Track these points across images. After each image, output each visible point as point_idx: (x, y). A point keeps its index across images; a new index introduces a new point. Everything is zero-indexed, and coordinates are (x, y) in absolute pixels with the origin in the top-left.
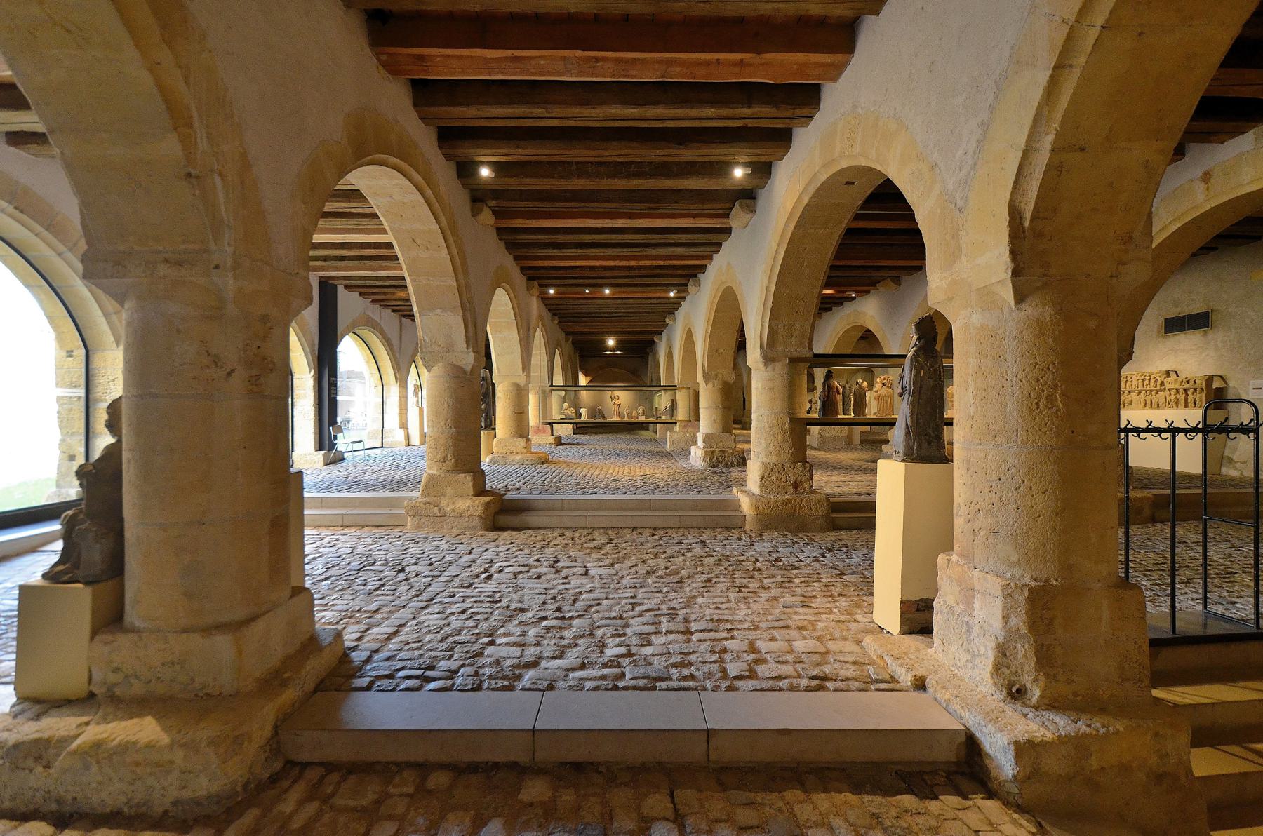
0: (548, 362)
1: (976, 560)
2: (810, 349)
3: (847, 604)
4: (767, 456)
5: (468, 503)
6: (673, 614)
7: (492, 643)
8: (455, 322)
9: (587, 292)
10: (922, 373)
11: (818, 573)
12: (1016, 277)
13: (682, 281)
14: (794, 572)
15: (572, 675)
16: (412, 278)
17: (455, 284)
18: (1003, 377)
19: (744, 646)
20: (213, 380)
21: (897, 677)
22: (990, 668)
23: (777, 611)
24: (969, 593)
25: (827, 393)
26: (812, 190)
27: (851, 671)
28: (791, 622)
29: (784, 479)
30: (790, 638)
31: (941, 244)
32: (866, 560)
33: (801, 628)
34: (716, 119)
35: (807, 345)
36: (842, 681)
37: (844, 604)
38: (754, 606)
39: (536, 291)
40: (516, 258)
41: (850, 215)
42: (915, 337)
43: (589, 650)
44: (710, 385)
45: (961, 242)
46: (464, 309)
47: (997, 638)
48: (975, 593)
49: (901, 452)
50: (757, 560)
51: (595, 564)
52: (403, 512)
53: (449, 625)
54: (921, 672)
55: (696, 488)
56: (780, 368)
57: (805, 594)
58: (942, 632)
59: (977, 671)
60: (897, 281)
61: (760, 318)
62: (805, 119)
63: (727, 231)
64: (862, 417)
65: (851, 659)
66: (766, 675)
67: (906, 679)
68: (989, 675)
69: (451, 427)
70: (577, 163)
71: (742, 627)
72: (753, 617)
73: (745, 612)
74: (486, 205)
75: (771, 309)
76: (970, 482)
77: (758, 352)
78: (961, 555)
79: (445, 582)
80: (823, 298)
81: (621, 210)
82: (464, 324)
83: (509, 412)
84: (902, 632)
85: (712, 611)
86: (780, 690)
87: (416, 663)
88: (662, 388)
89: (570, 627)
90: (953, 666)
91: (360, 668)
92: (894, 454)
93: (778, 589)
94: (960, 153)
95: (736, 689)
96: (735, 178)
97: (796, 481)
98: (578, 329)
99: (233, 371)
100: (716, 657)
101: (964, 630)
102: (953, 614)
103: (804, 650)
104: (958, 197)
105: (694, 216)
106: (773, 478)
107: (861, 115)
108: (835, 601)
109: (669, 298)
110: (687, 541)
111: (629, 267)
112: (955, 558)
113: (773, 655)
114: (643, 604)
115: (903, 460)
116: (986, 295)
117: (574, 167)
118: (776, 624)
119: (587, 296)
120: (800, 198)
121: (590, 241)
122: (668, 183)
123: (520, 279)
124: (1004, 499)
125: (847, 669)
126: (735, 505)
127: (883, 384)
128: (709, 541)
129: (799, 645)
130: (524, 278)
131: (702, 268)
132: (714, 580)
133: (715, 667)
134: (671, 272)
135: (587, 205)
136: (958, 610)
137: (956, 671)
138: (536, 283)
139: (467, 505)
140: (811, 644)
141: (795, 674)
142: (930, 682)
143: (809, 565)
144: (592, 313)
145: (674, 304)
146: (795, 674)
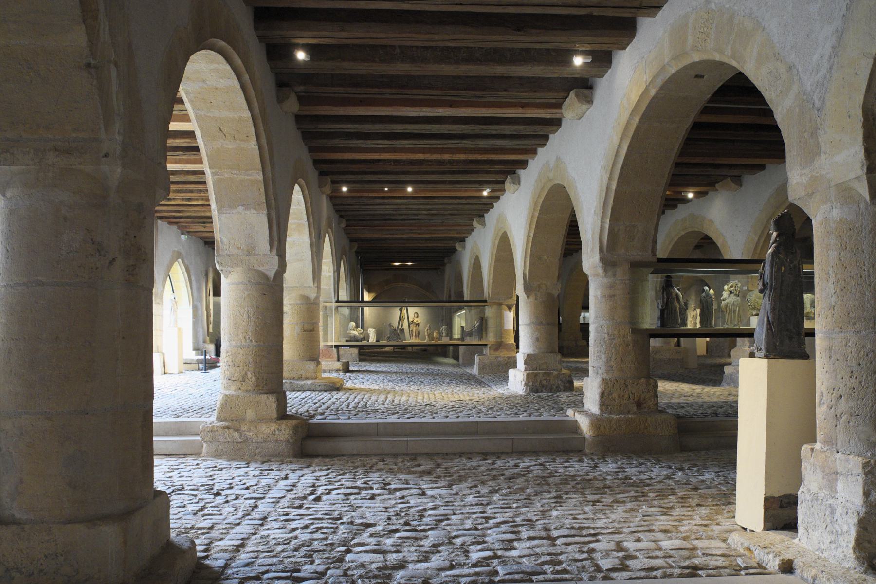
0: (334, 272)
1: (839, 444)
2: (654, 252)
3: (707, 512)
4: (607, 372)
5: (274, 426)
6: (530, 524)
7: (348, 551)
8: (259, 221)
9: (386, 189)
10: (783, 268)
11: (672, 489)
12: (871, 173)
13: (498, 178)
14: (647, 488)
15: (443, 574)
16: (213, 171)
17: (261, 177)
18: (861, 268)
19: (612, 546)
20: (97, 268)
21: (764, 565)
22: (852, 543)
23: (638, 519)
24: (832, 476)
25: (665, 300)
26: (659, 82)
27: (721, 561)
28: (654, 527)
29: (626, 396)
30: (656, 539)
31: (800, 142)
32: (720, 477)
33: (665, 531)
34: (561, 6)
35: (650, 248)
36: (713, 569)
37: (704, 512)
38: (613, 516)
39: (328, 189)
40: (311, 150)
41: (698, 109)
42: (775, 234)
43: (453, 554)
44: (532, 299)
45: (820, 140)
46: (269, 207)
47: (858, 514)
48: (838, 476)
49: (763, 348)
50: (605, 479)
51: (431, 486)
52: (198, 438)
53: (296, 538)
54: (787, 556)
55: (525, 411)
56: (622, 273)
57: (663, 505)
58: (806, 520)
59: (840, 550)
60: (738, 181)
61: (600, 218)
62: (653, 9)
63: (556, 123)
64: (709, 327)
65: (719, 552)
66: (638, 567)
67: (773, 564)
68: (851, 551)
69: (251, 341)
70: (400, 47)
71: (605, 532)
72: (616, 525)
73: (605, 521)
74: (293, 90)
75: (612, 208)
76: (832, 370)
77: (597, 257)
78: (825, 442)
79: (272, 503)
80: (667, 199)
81: (444, 98)
82: (269, 223)
83: (297, 330)
84: (767, 528)
85: (570, 521)
86: (655, 577)
87: (280, 567)
88: (465, 304)
89: (427, 537)
90: (817, 550)
91: (222, 573)
92: (756, 351)
93: (633, 503)
94: (816, 57)
95: (612, 579)
96: (576, 67)
97: (639, 399)
98: (367, 234)
99: (114, 260)
100: (585, 556)
101: (827, 513)
102: (817, 500)
103: (673, 547)
104: (815, 98)
105: (523, 106)
106: (615, 395)
107: (715, 11)
108: (694, 511)
109: (483, 197)
110: (524, 464)
111: (440, 161)
112: (818, 446)
113: (642, 553)
114: (495, 518)
115: (766, 356)
116: (845, 193)
117: (398, 50)
118: (640, 529)
119: (386, 195)
120: (646, 90)
121: (401, 131)
122: (500, 70)
123: (313, 174)
124: (863, 383)
125: (716, 560)
126: (574, 427)
127: (731, 292)
128: (548, 464)
129: (666, 544)
130: (317, 173)
131: (523, 164)
132: (565, 497)
133: (587, 563)
134: (487, 167)
135: (406, 91)
136: (821, 495)
137: (821, 554)
138: (329, 179)
139: (272, 428)
140: (677, 543)
141: (668, 566)
142: (797, 563)
143: (661, 482)
144: (387, 215)
145: (485, 204)
146: (668, 566)
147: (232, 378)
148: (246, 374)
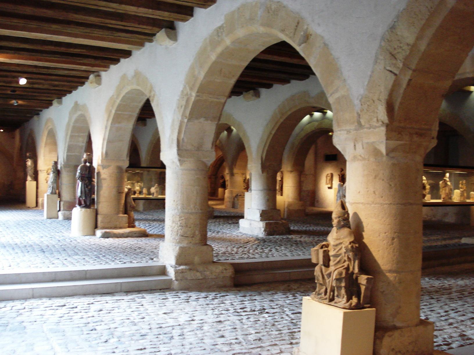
147: (185, 235)
148: (195, 232)
